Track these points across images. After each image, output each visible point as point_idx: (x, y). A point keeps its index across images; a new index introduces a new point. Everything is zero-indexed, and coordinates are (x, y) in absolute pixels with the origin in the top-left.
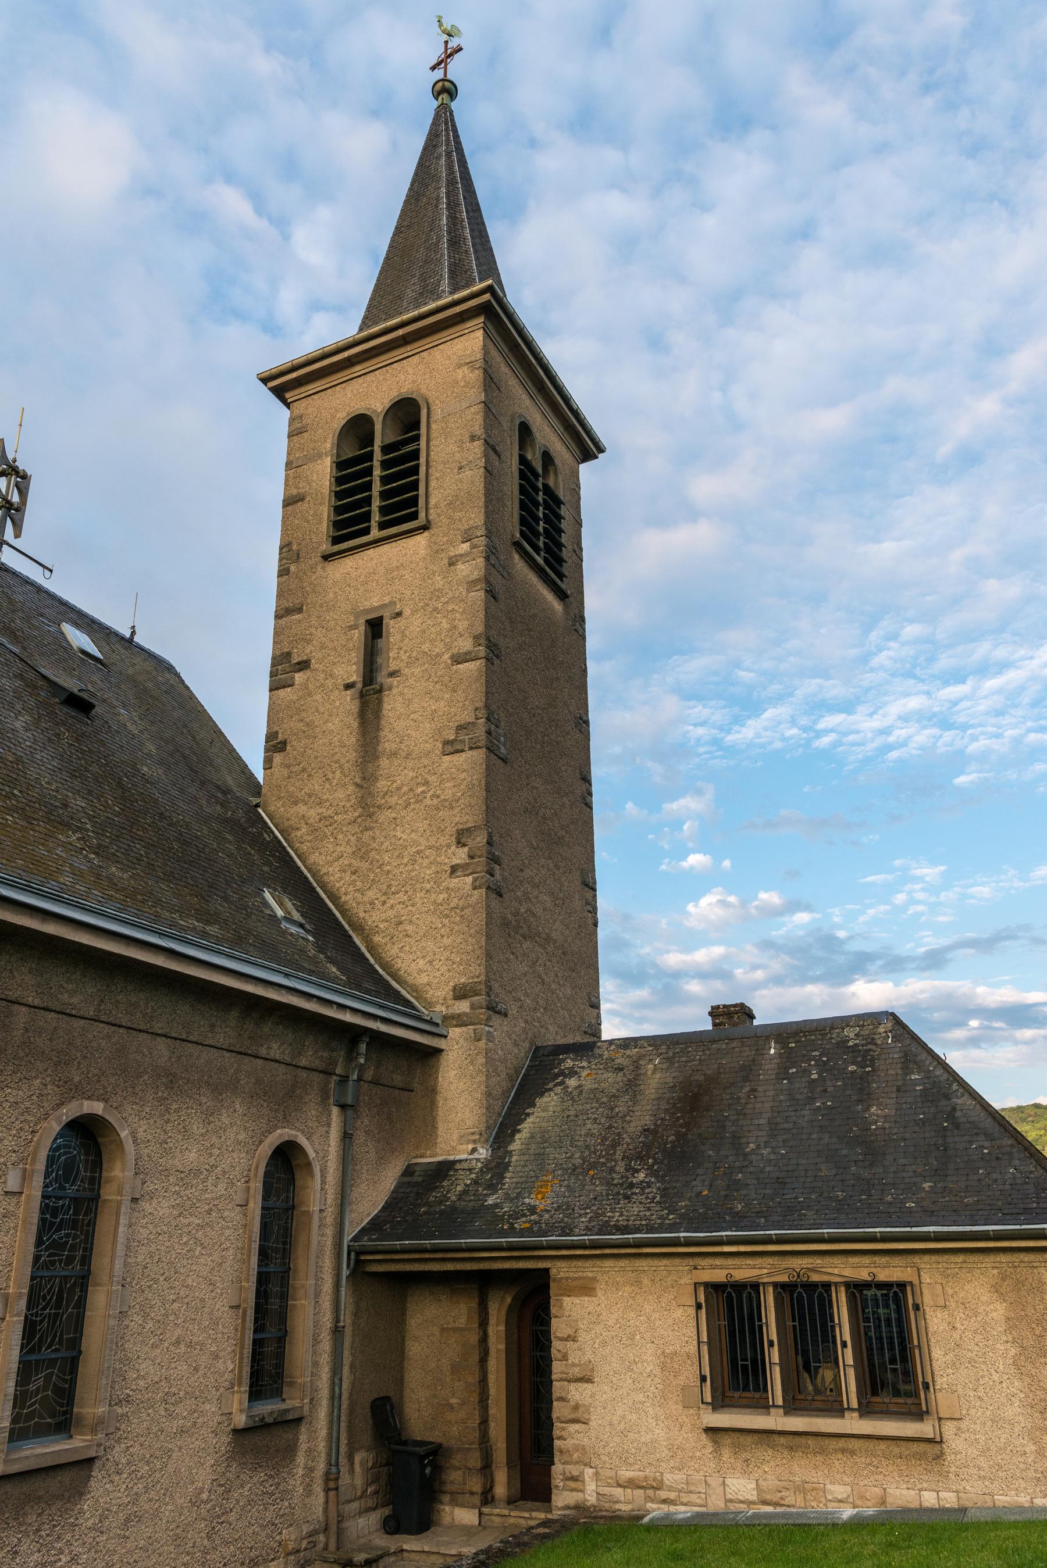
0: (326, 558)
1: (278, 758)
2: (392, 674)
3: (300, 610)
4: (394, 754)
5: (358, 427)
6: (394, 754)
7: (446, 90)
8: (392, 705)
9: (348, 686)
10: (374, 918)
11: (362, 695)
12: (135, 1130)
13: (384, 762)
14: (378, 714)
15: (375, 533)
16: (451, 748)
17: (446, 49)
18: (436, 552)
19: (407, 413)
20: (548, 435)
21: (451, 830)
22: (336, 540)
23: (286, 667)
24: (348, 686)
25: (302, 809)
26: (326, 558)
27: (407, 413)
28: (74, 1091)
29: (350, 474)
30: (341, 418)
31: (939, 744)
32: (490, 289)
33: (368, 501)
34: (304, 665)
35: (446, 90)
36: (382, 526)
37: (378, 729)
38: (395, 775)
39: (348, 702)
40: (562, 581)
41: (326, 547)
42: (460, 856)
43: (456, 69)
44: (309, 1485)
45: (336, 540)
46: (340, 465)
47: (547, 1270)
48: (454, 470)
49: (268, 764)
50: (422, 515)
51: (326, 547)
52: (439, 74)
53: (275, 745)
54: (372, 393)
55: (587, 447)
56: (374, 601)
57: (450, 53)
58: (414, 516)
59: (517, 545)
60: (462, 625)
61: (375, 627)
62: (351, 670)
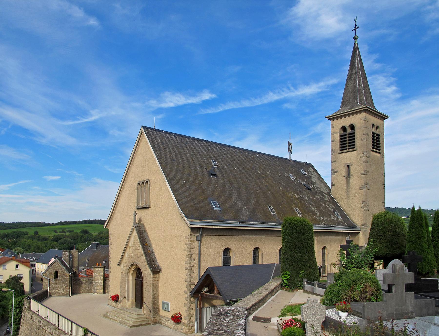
0: (339, 153)
1: (333, 187)
2: (351, 175)
3: (335, 162)
4: (352, 188)
6: (352, 188)
8: (352, 180)
9: (344, 176)
10: (350, 213)
11: (347, 178)
12: (328, 247)
13: (350, 189)
14: (349, 182)
16: (361, 188)
18: (358, 155)
19: (352, 127)
21: (361, 201)
23: (334, 172)
24: (344, 176)
25: (338, 195)
27: (352, 127)
28: (323, 244)
29: (342, 137)
30: (341, 126)
31: (222, 326)
33: (346, 138)
34: (336, 172)
36: (349, 149)
37: (349, 184)
38: (353, 192)
39: (344, 179)
42: (362, 205)
45: (341, 150)
46: (341, 136)
47: (437, 280)
48: (361, 139)
49: (332, 187)
51: (339, 151)
53: (333, 185)
54: (346, 122)
56: (348, 162)
58: (354, 148)
59: (372, 150)
60: (362, 168)
61: (348, 166)
62: (344, 173)
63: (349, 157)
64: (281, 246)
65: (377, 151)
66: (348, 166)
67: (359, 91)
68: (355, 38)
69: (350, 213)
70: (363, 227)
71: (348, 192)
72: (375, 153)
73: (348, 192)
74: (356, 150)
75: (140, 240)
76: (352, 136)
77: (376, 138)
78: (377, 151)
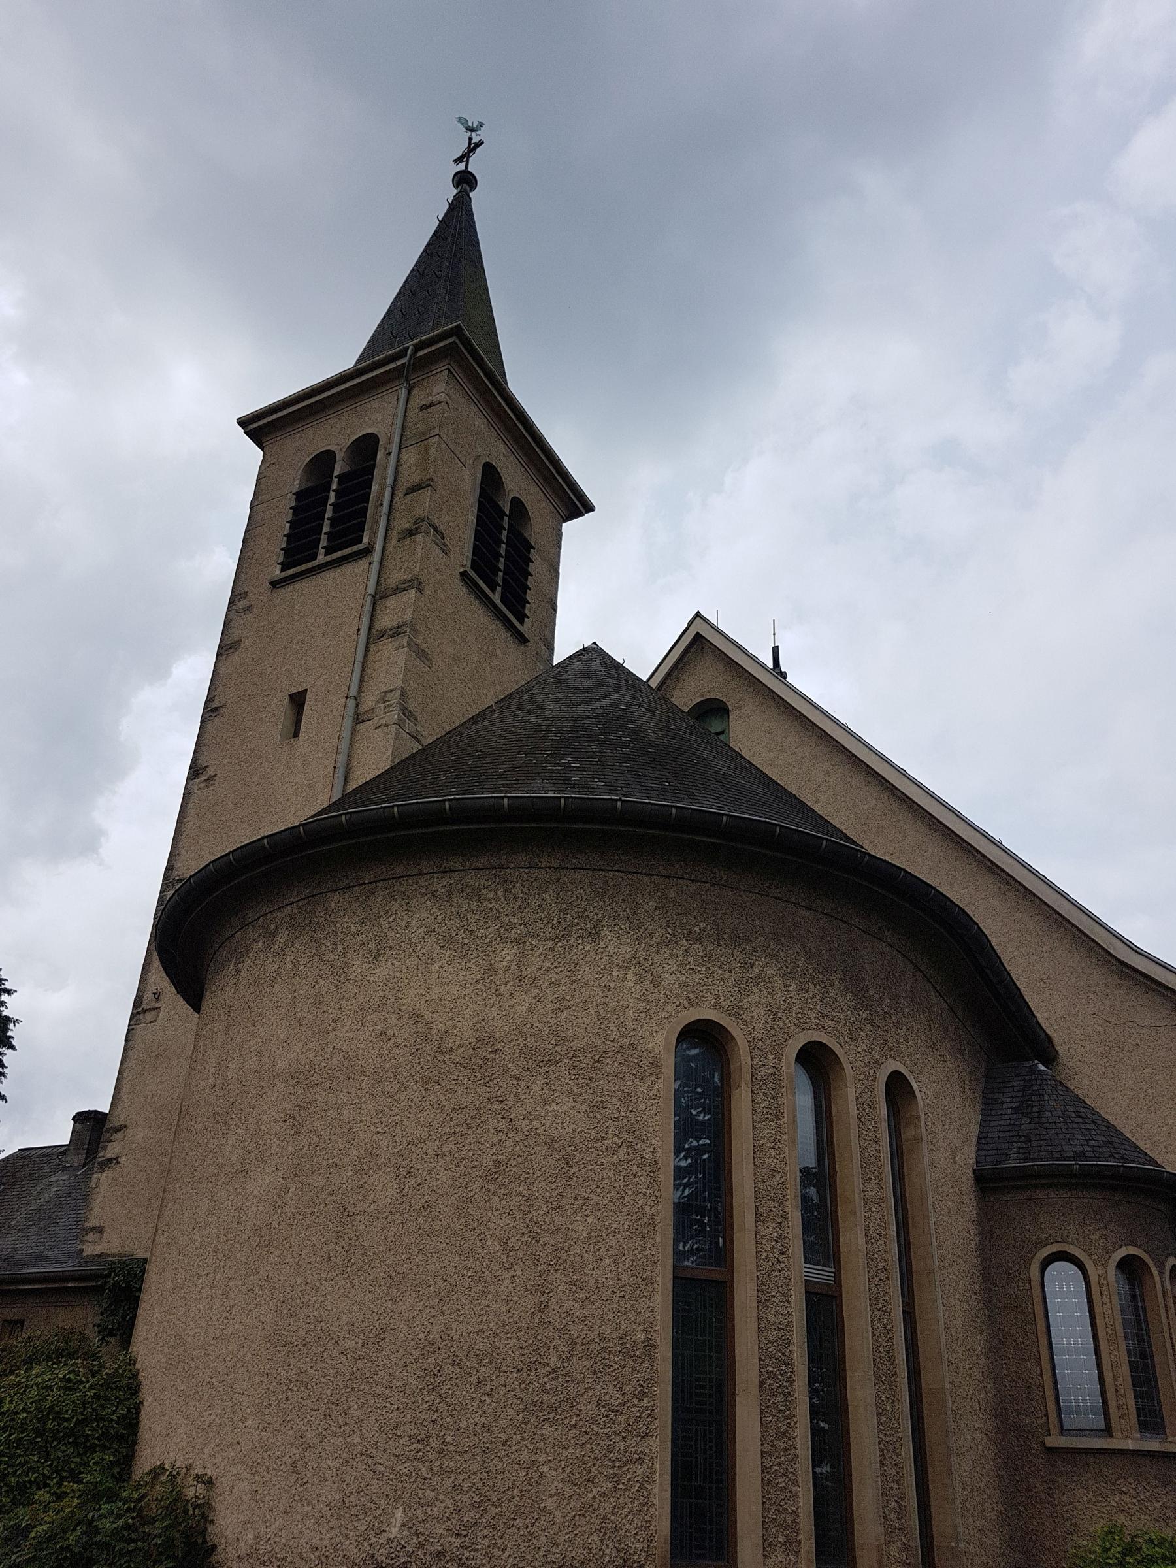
0: (275, 584)
5: (323, 461)
7: (465, 181)
15: (321, 557)
17: (470, 144)
20: (518, 482)
22: (285, 566)
26: (275, 584)
29: (307, 505)
32: (457, 331)
35: (465, 181)
40: (522, 622)
41: (277, 573)
43: (475, 165)
44: (10, 1540)
50: (365, 540)
51: (277, 573)
52: (462, 166)
55: (575, 504)
57: (473, 147)
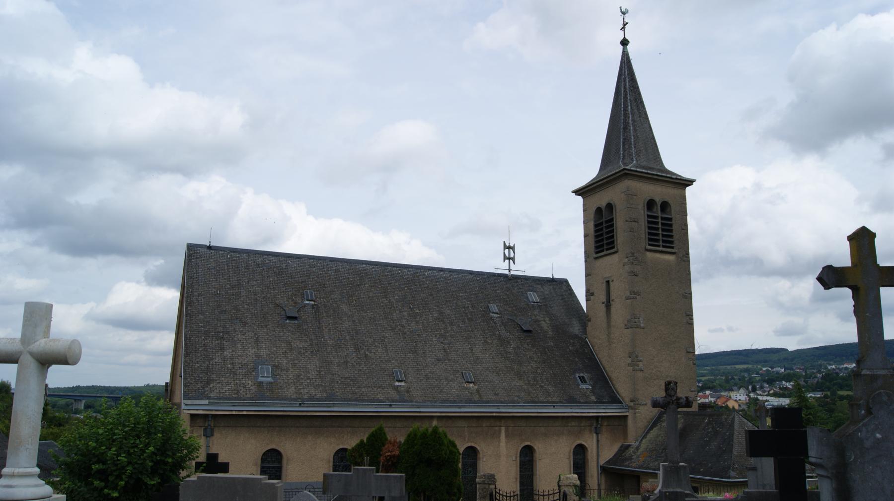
0: (596, 258)
8: (613, 310)
19: (192, 416)
27: (610, 207)
45: (597, 253)
46: (596, 226)
58: (613, 247)
61: (608, 282)
62: (603, 298)
63: (612, 264)
64: (349, 448)
65: (664, 249)
66: (608, 282)
67: (624, 139)
68: (625, 42)
69: (614, 376)
70: (632, 404)
71: (609, 334)
72: (658, 255)
73: (609, 334)
74: (616, 252)
75: (43, 304)
76: (610, 223)
77: (660, 226)
78: (664, 249)
